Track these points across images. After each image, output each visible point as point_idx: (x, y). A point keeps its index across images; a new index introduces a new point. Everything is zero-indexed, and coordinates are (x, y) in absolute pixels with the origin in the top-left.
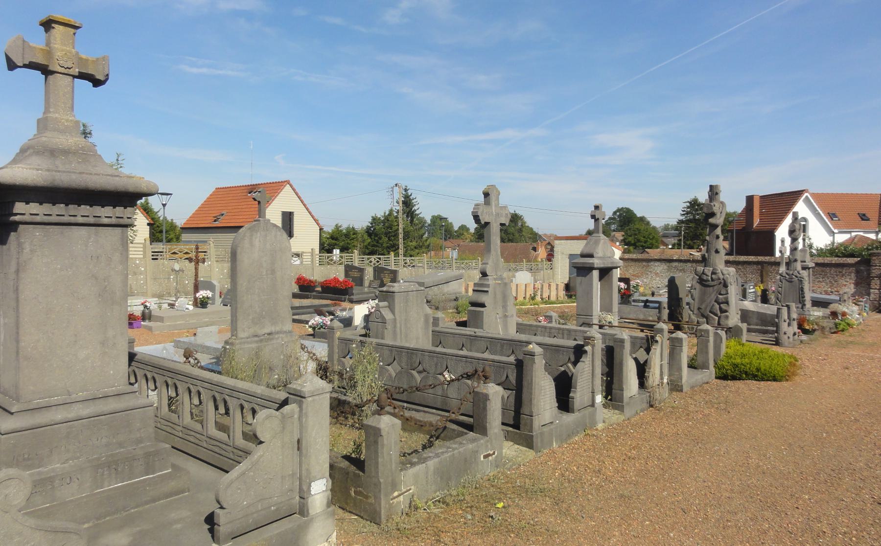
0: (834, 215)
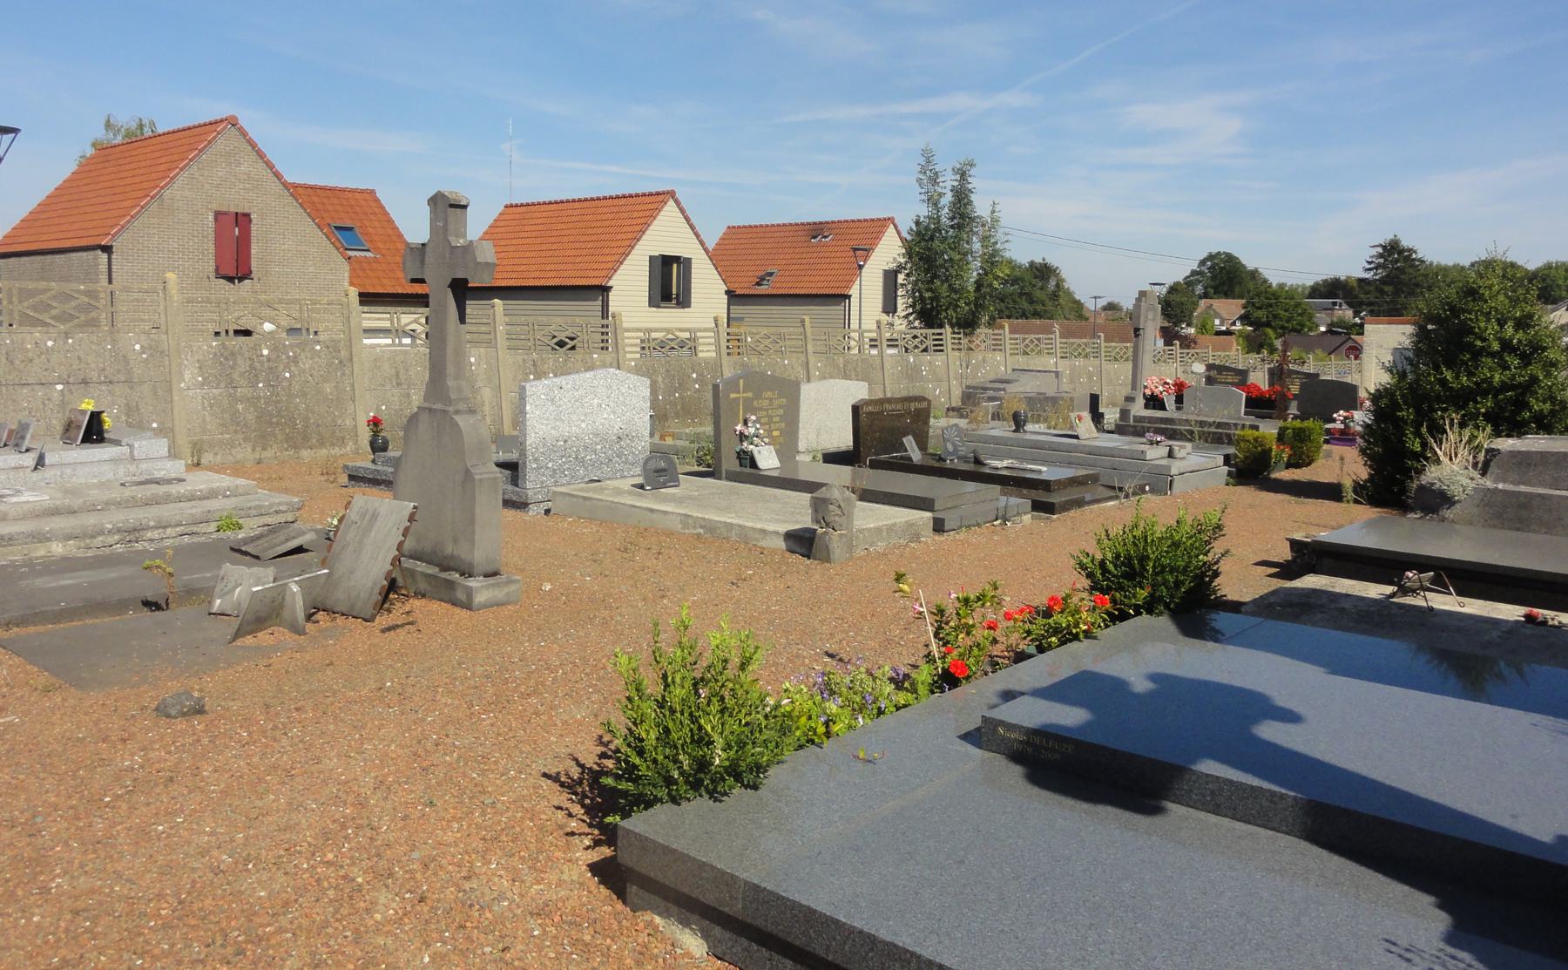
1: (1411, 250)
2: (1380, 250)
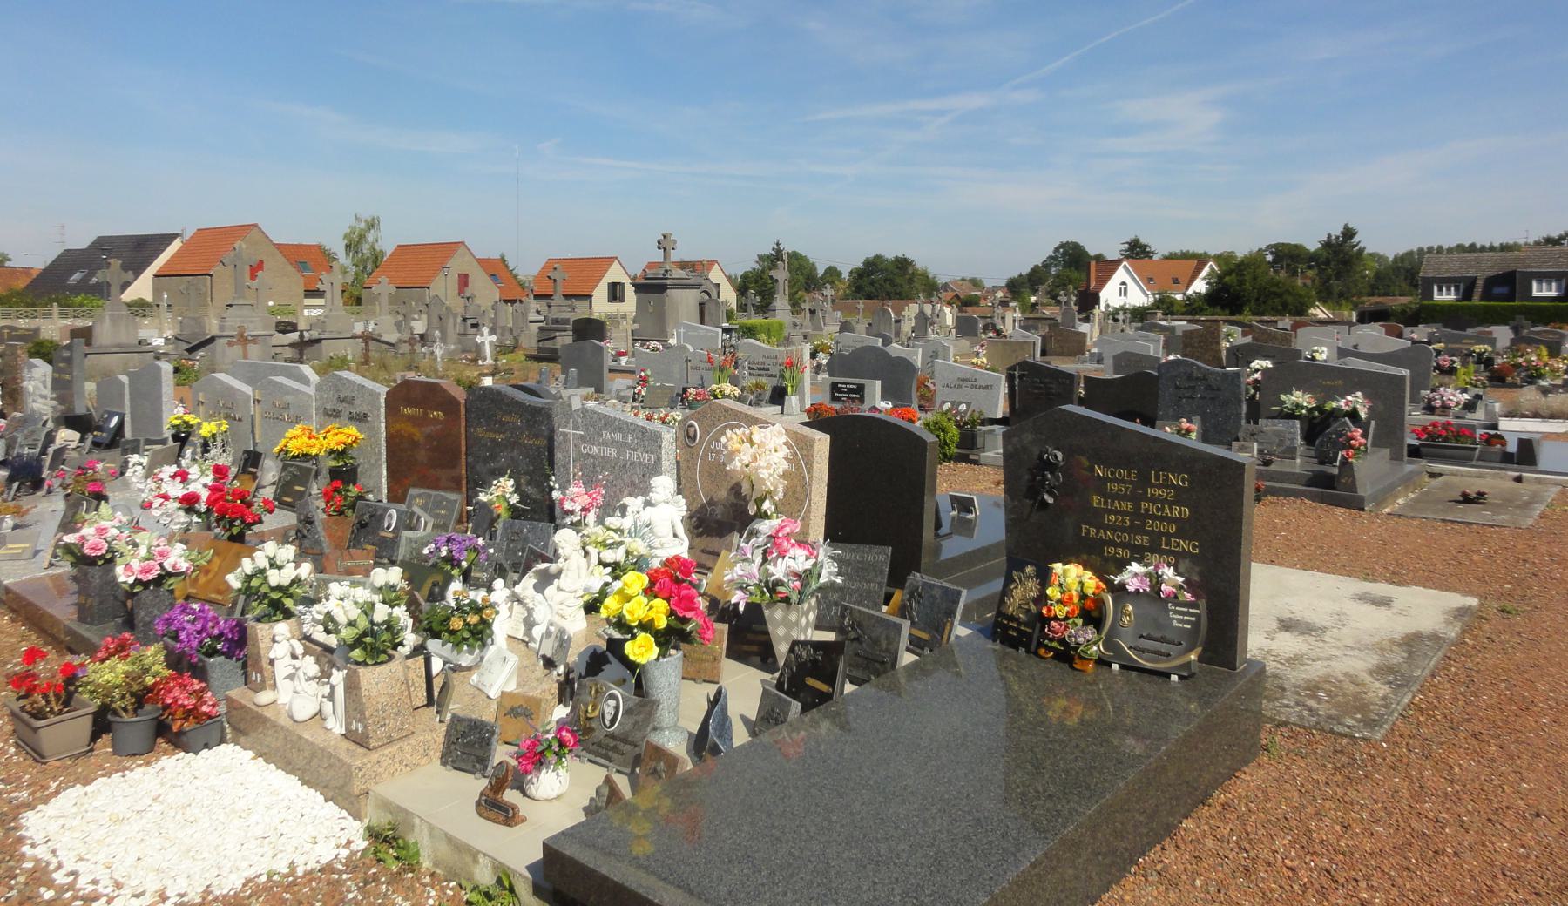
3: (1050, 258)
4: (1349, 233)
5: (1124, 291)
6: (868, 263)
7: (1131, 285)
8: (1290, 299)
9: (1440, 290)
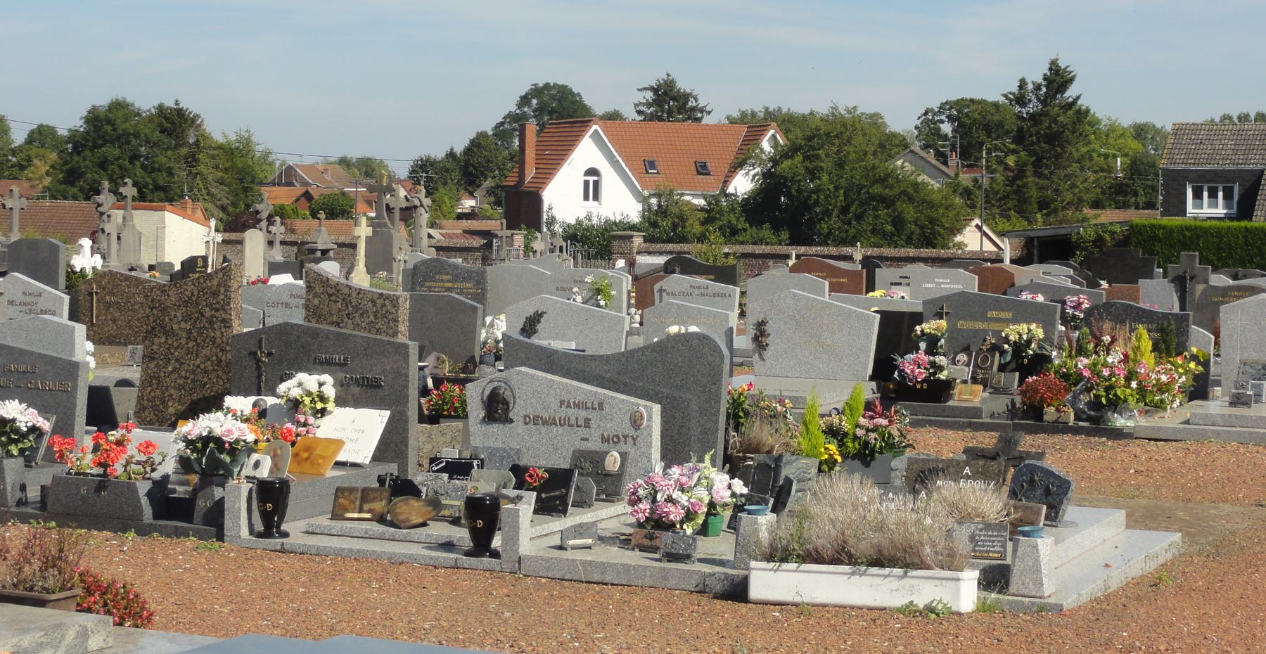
0: (652, 164)
1: (686, 97)
2: (649, 95)
3: (512, 118)
4: (1058, 79)
5: (593, 190)
6: (96, 119)
7: (611, 182)
8: (909, 212)
9: (1198, 195)
